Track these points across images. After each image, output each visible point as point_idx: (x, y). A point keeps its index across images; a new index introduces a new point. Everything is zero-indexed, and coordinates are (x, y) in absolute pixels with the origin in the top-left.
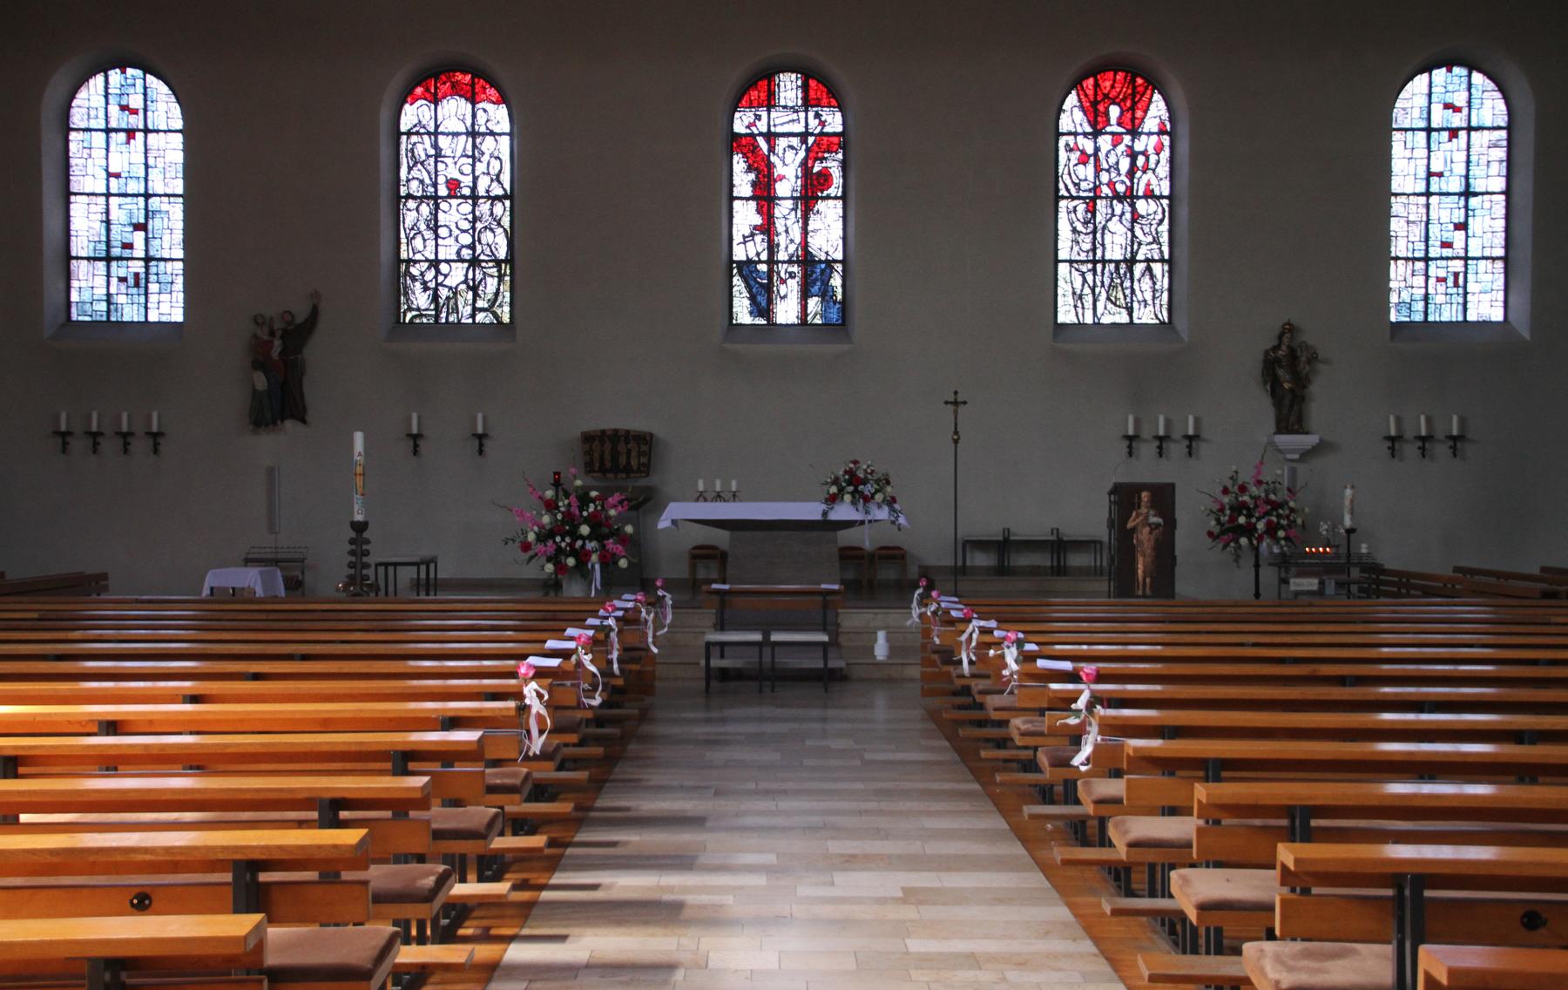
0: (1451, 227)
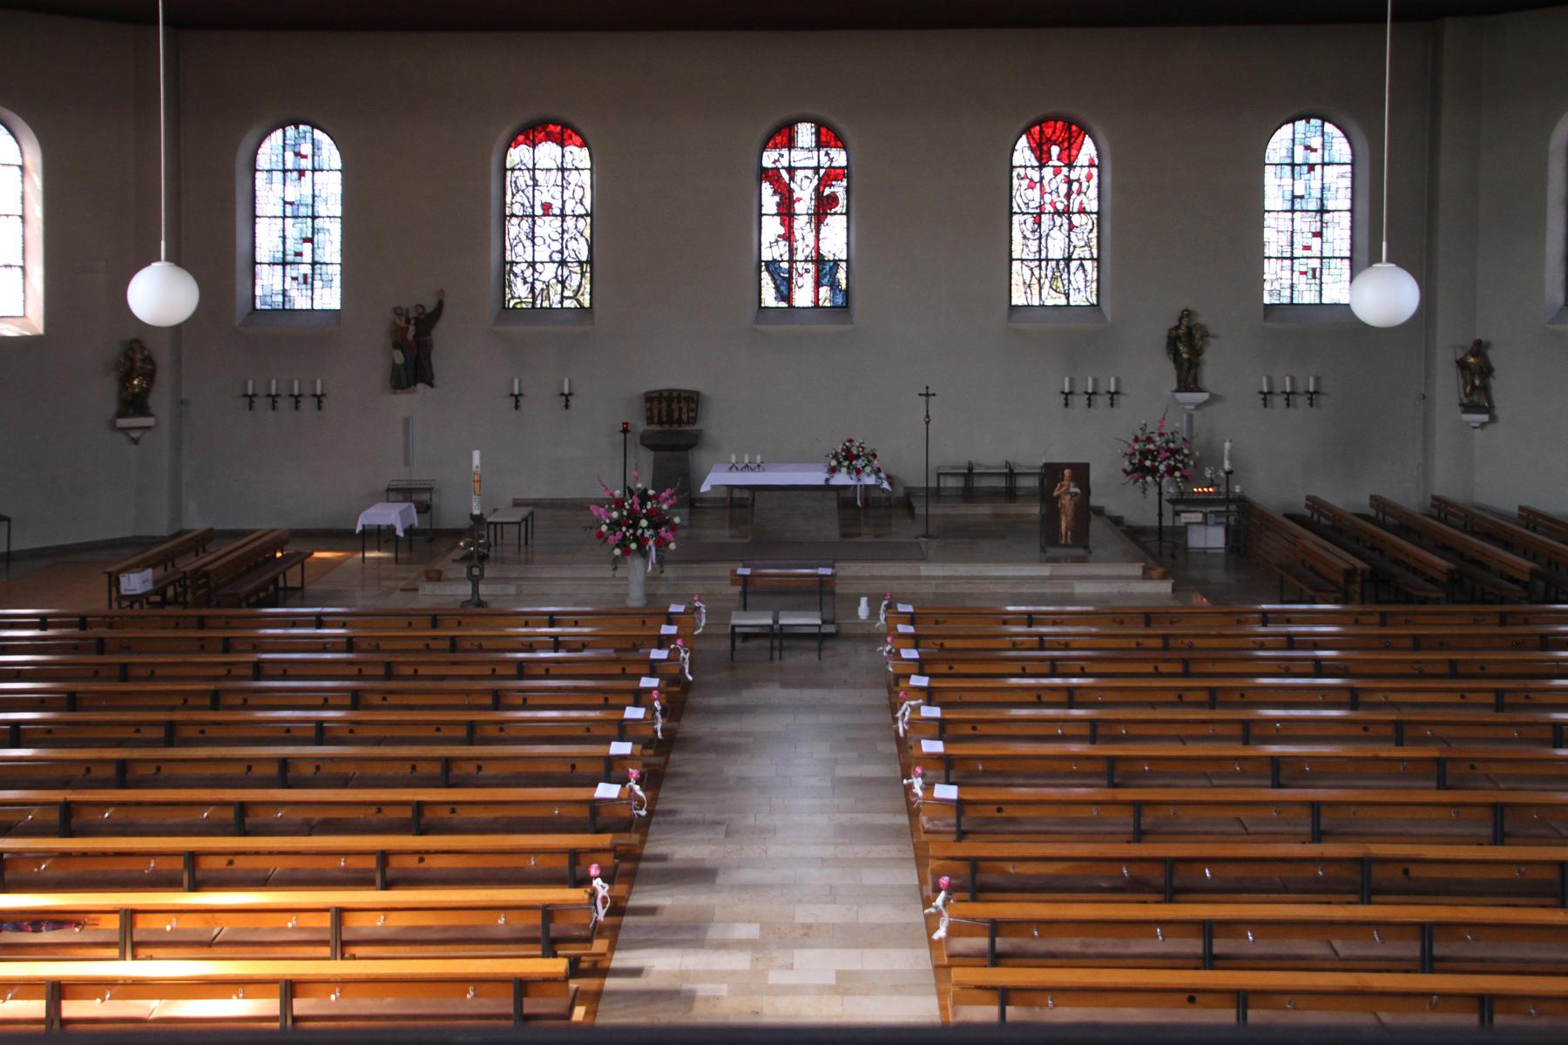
0: (1310, 235)
